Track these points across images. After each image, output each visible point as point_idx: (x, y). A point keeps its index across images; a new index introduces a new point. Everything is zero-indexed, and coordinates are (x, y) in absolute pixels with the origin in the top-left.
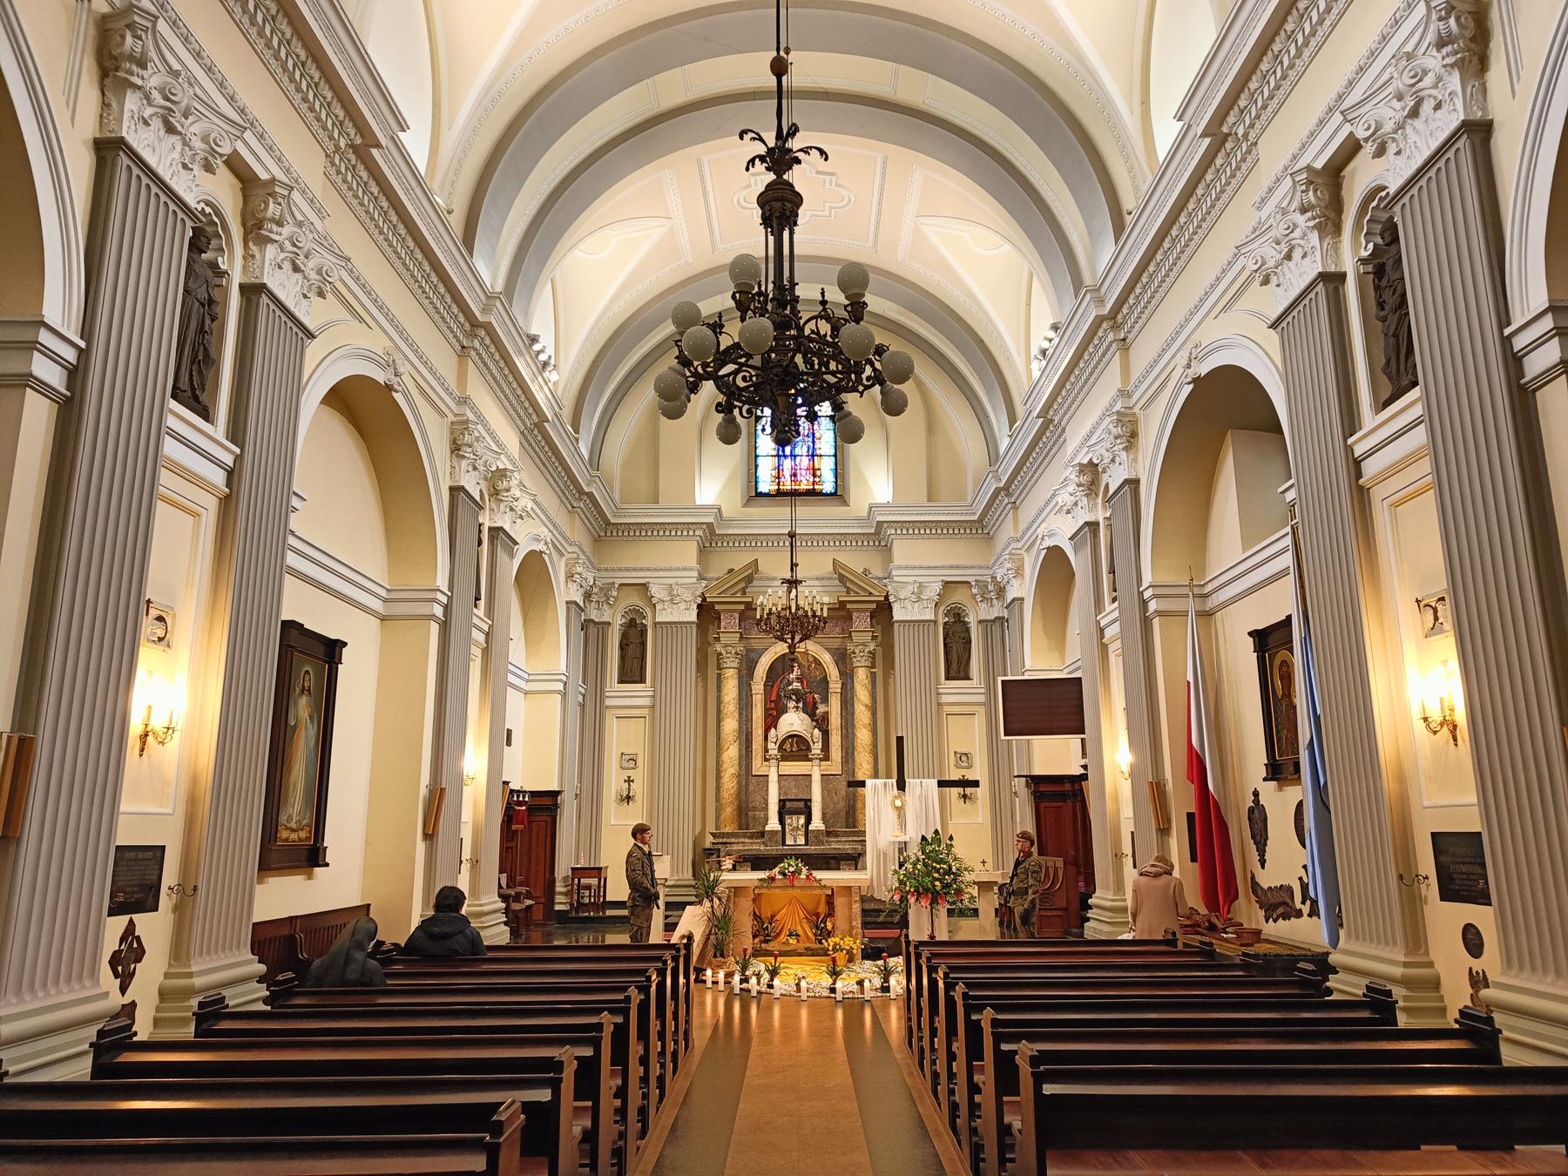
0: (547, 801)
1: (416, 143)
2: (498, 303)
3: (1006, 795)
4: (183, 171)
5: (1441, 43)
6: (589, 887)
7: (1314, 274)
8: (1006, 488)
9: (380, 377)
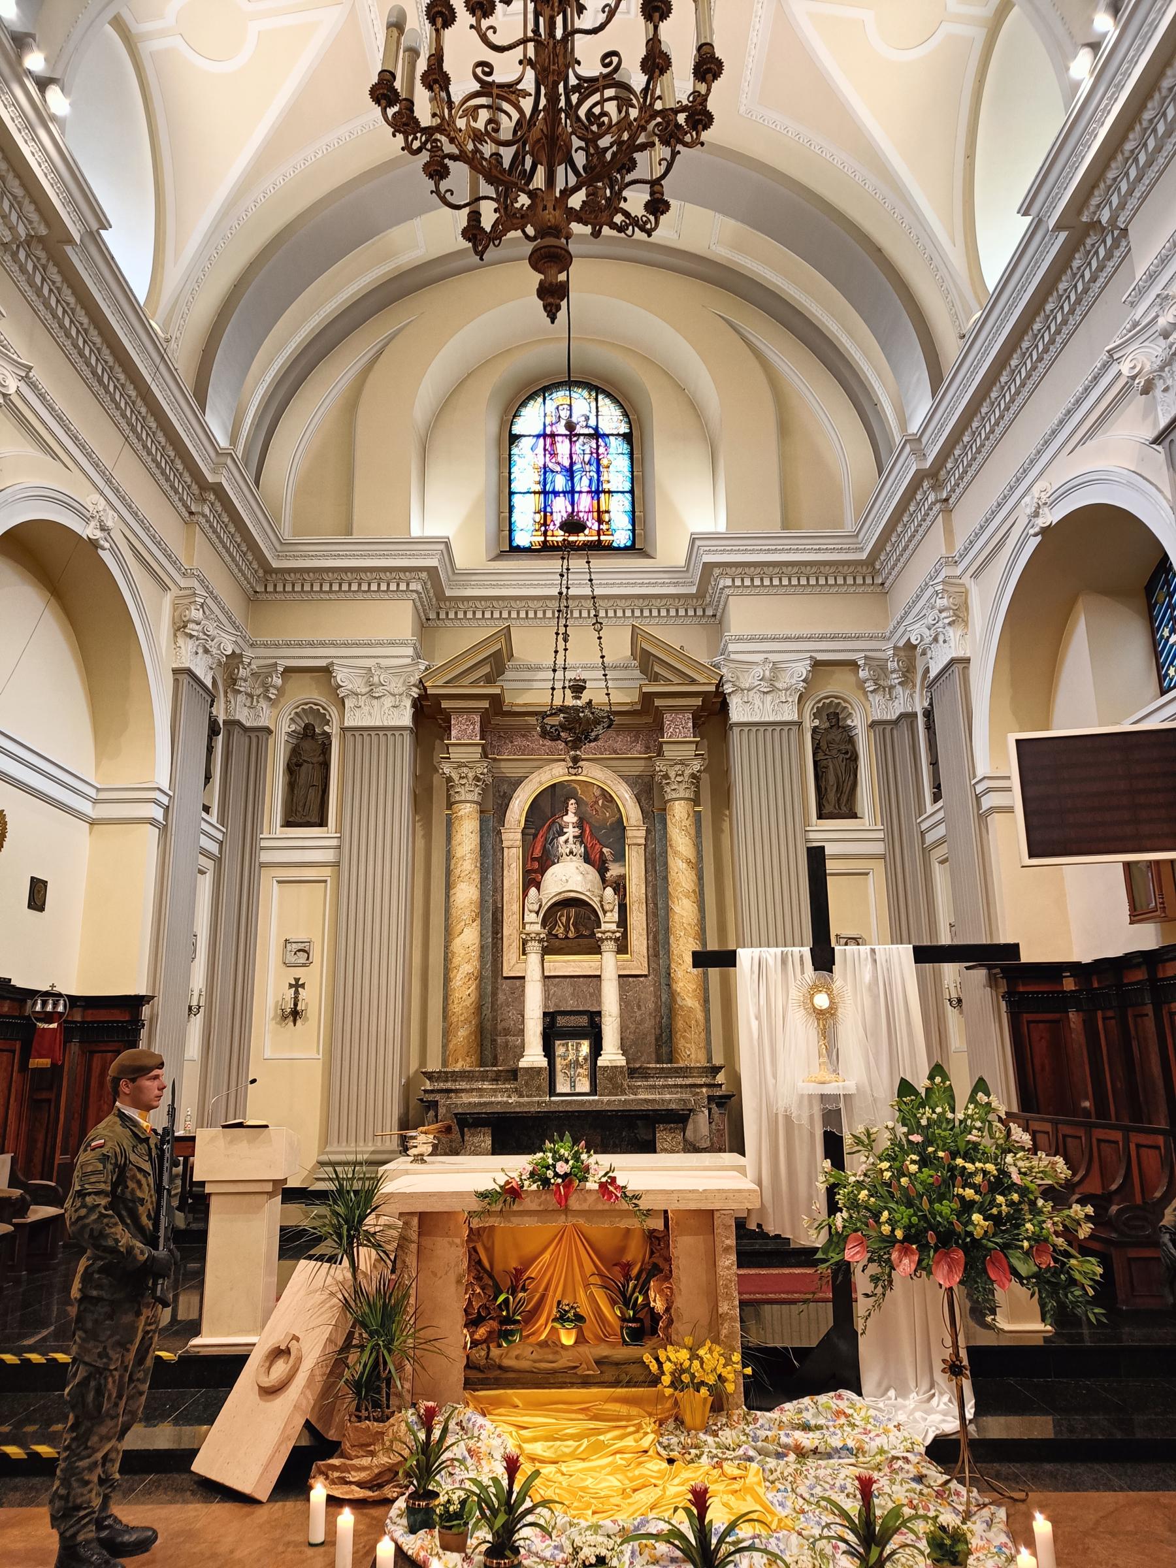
1: (130, 249)
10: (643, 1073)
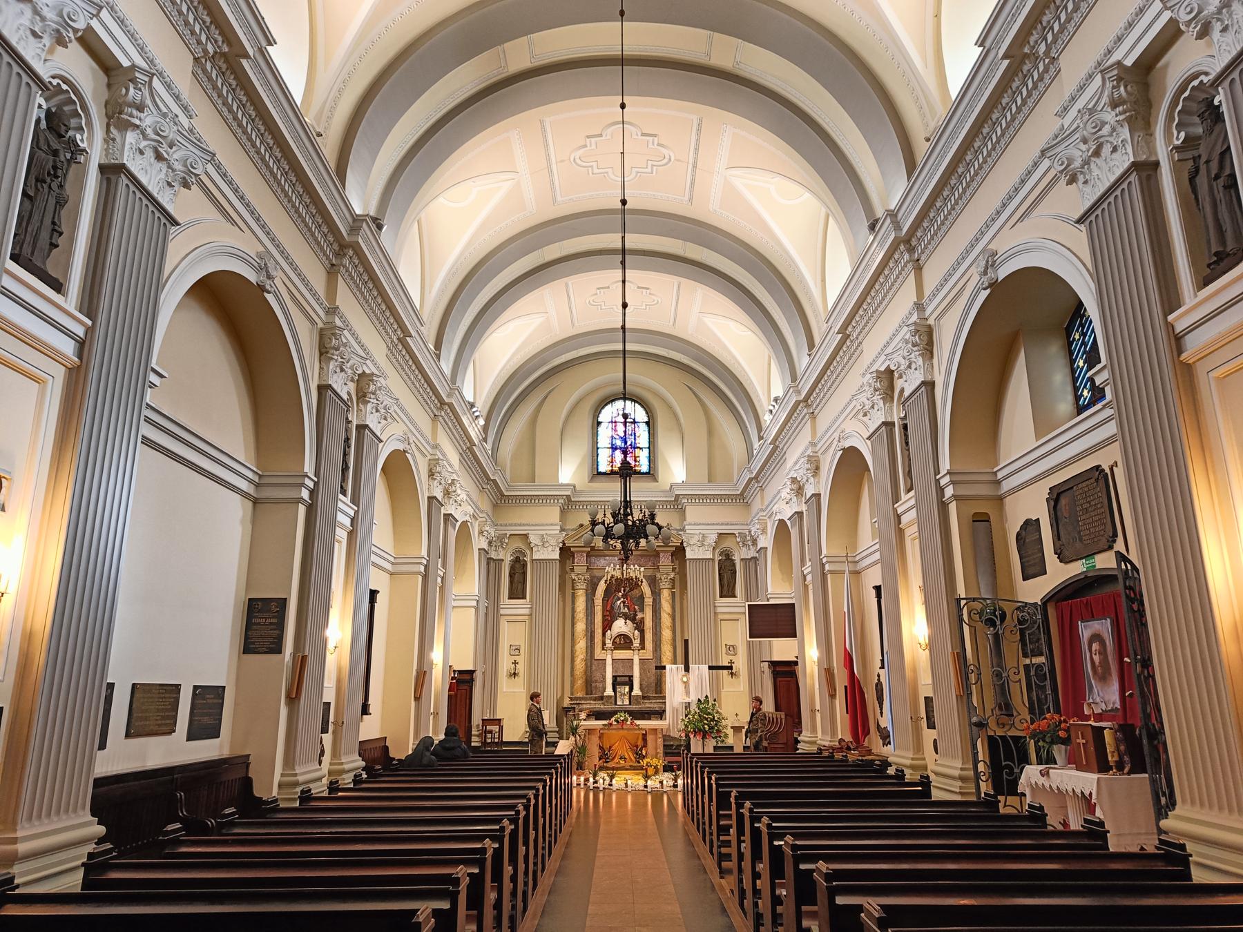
0: (467, 677)
1: (290, 62)
2: (364, 225)
3: (758, 673)
4: (31, 38)
5: (1114, 104)
6: (491, 732)
7: (918, 382)
8: (756, 477)
9: (252, 276)
10: (648, 698)
